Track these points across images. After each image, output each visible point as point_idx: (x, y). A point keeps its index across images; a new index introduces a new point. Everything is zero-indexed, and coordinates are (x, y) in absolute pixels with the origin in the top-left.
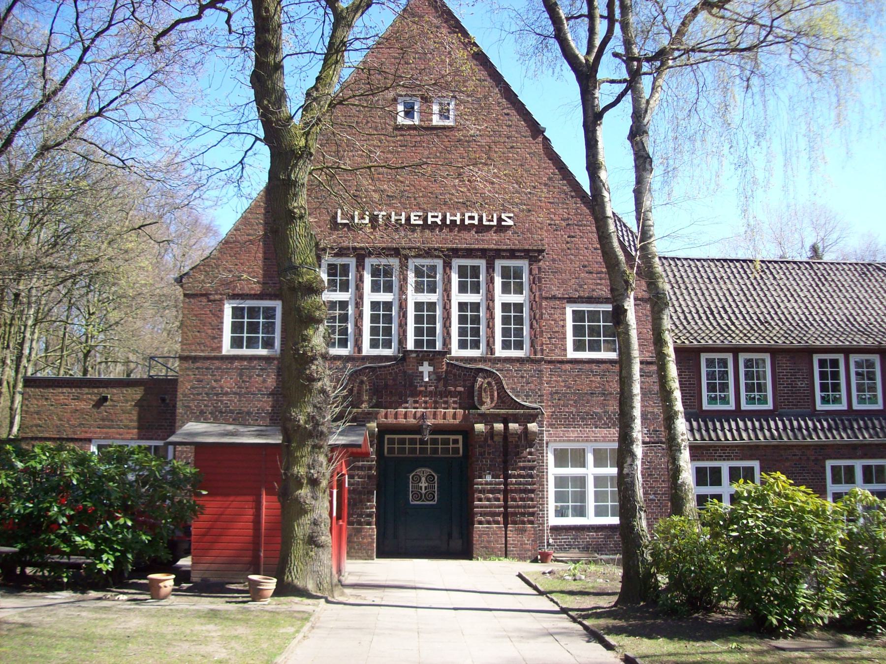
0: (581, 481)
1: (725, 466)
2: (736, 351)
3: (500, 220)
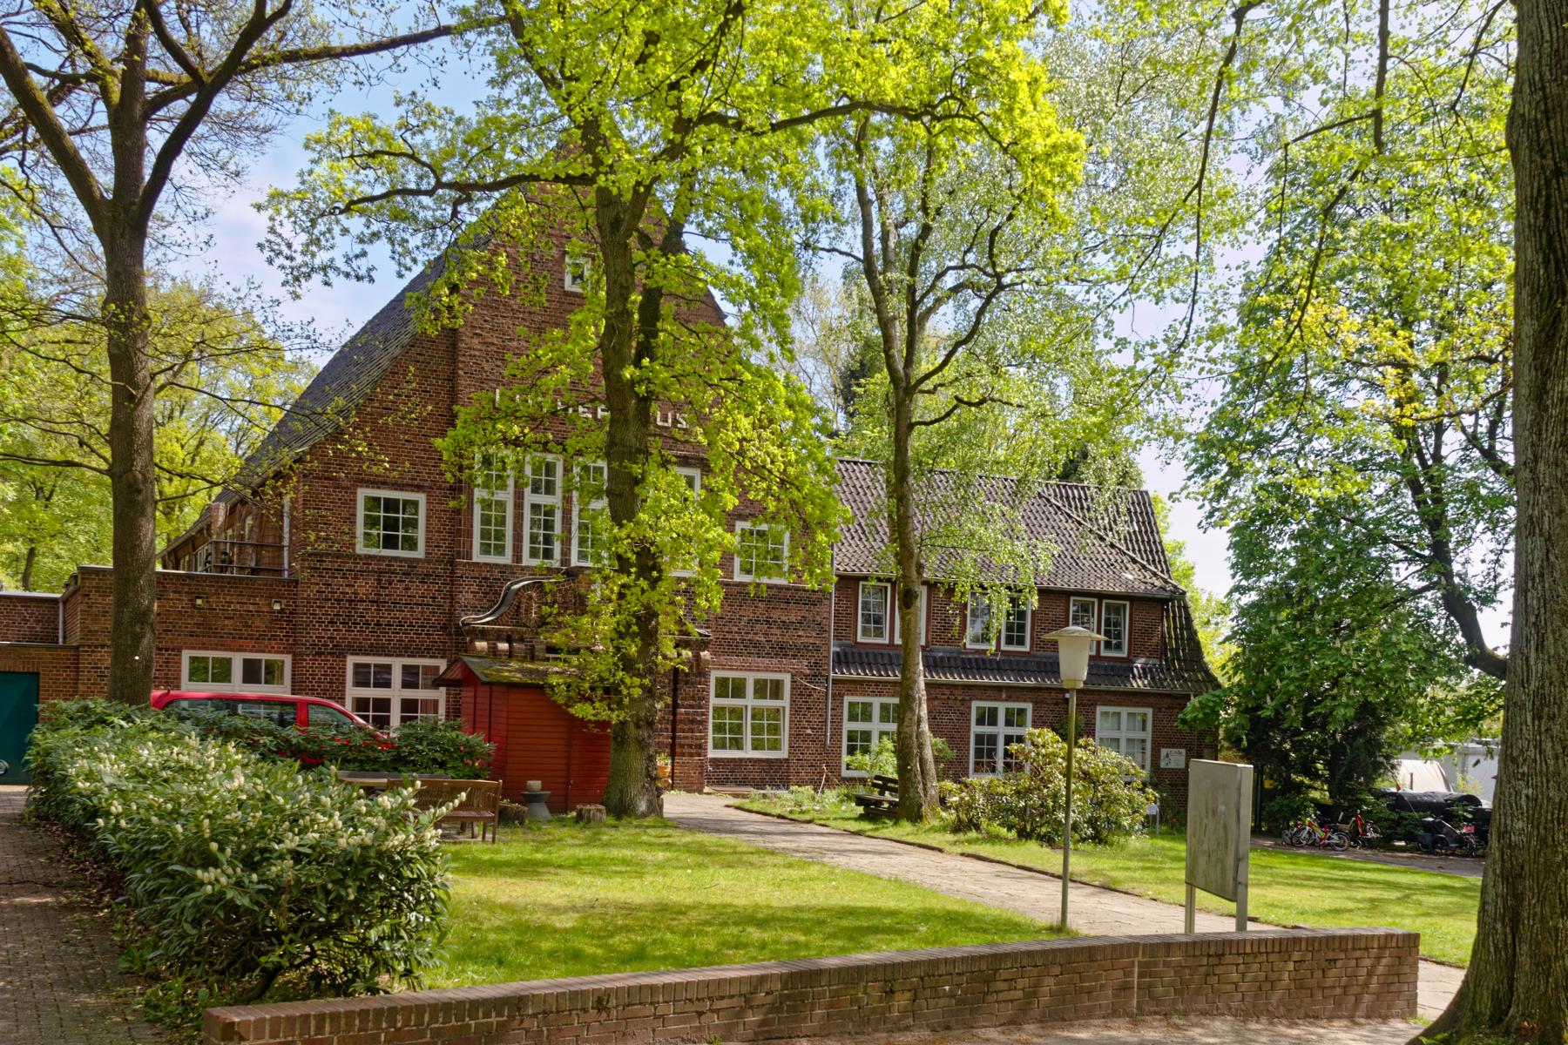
0: (992, 739)
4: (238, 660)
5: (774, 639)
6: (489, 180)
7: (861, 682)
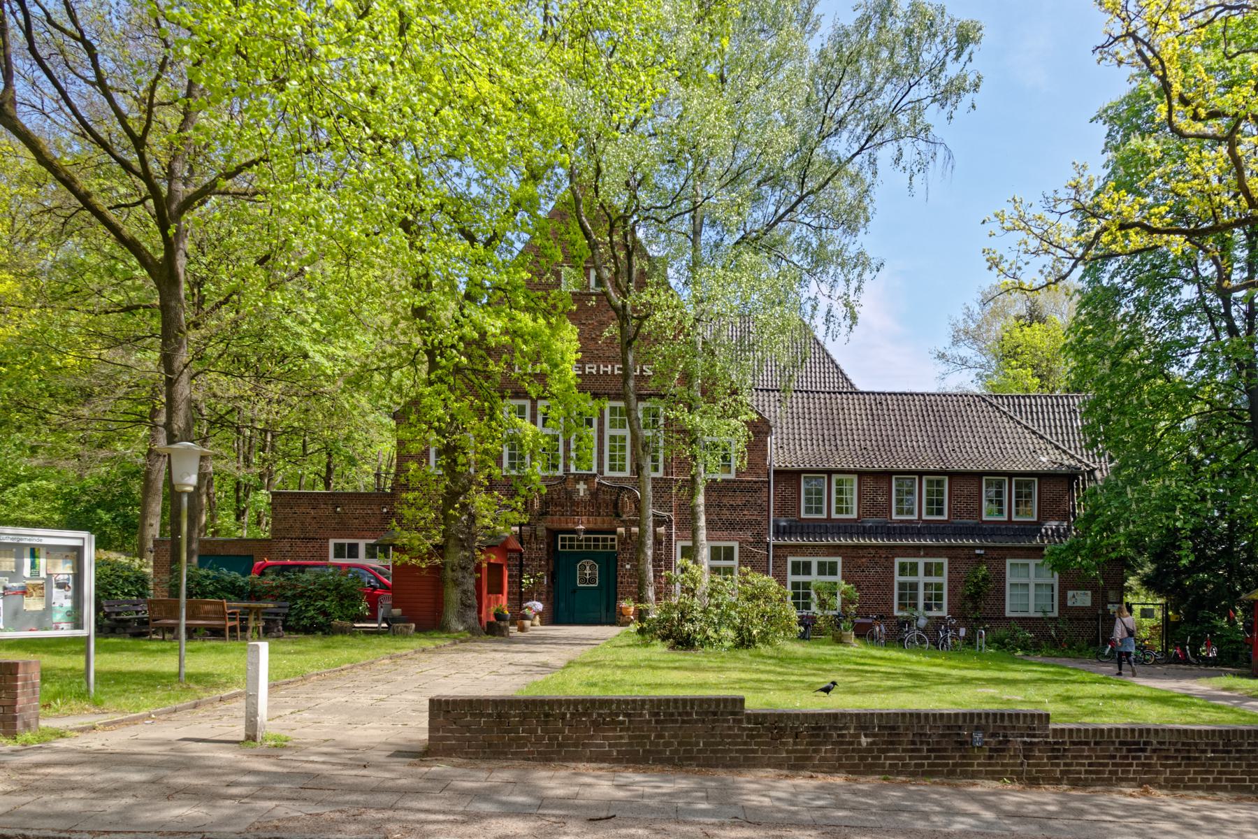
0: (914, 586)
1: (814, 561)
2: (830, 472)
3: (642, 371)
4: (362, 544)
5: (724, 518)
6: (145, 116)
7: (801, 546)
